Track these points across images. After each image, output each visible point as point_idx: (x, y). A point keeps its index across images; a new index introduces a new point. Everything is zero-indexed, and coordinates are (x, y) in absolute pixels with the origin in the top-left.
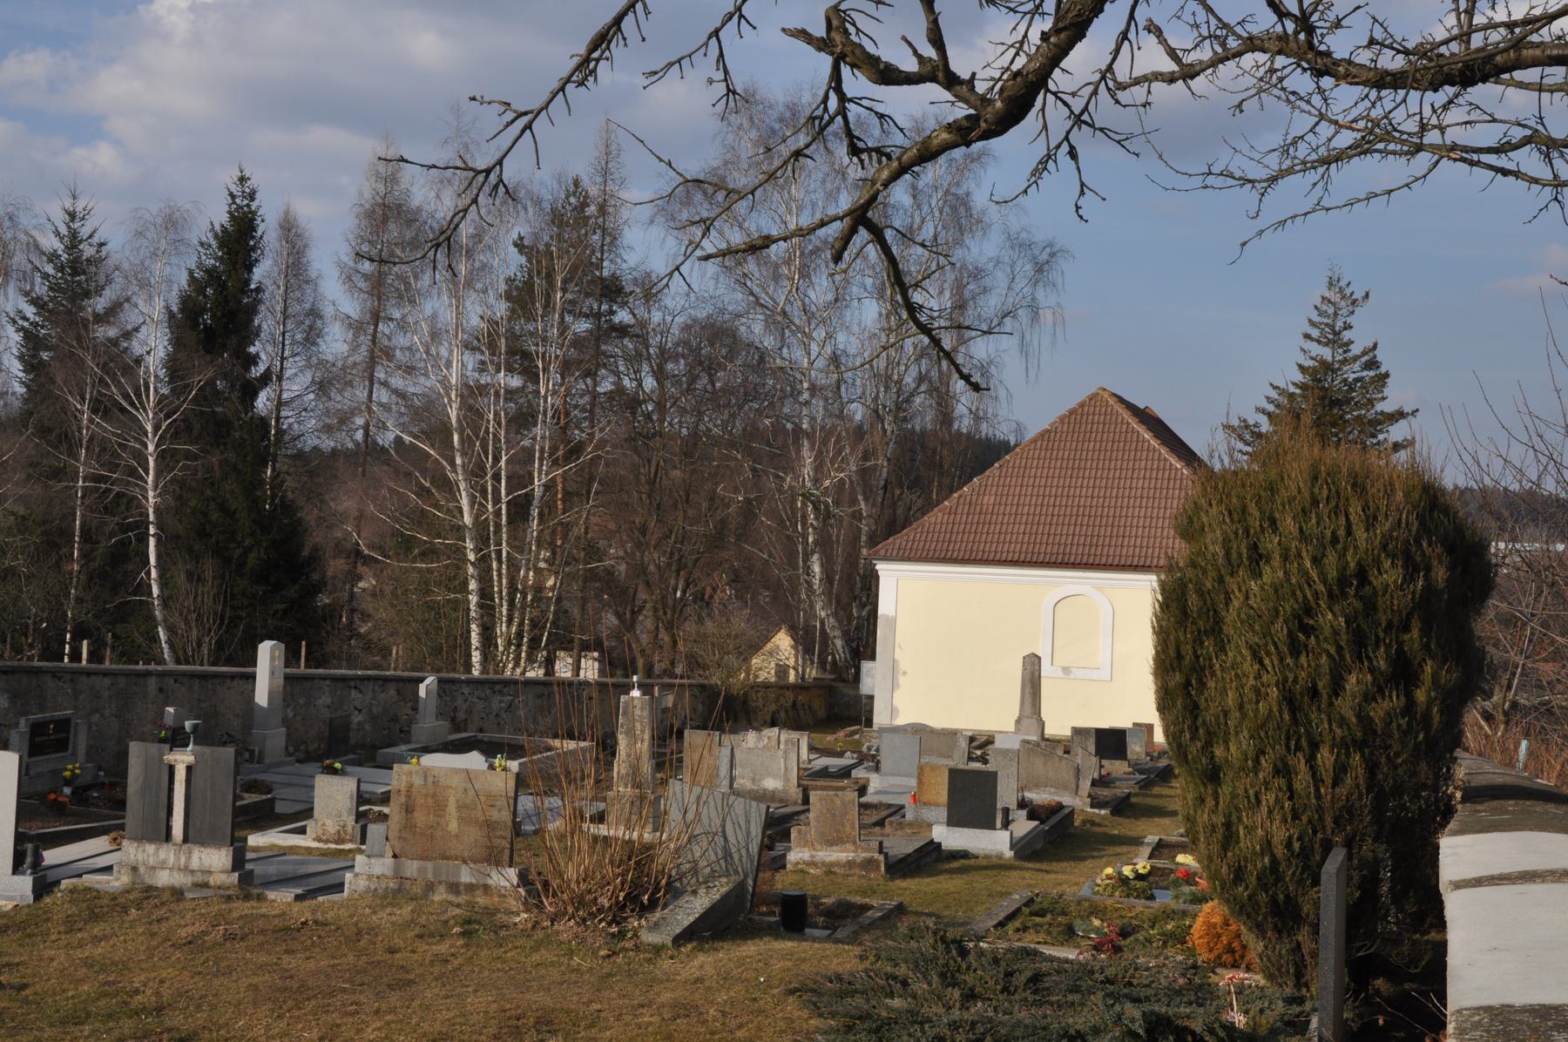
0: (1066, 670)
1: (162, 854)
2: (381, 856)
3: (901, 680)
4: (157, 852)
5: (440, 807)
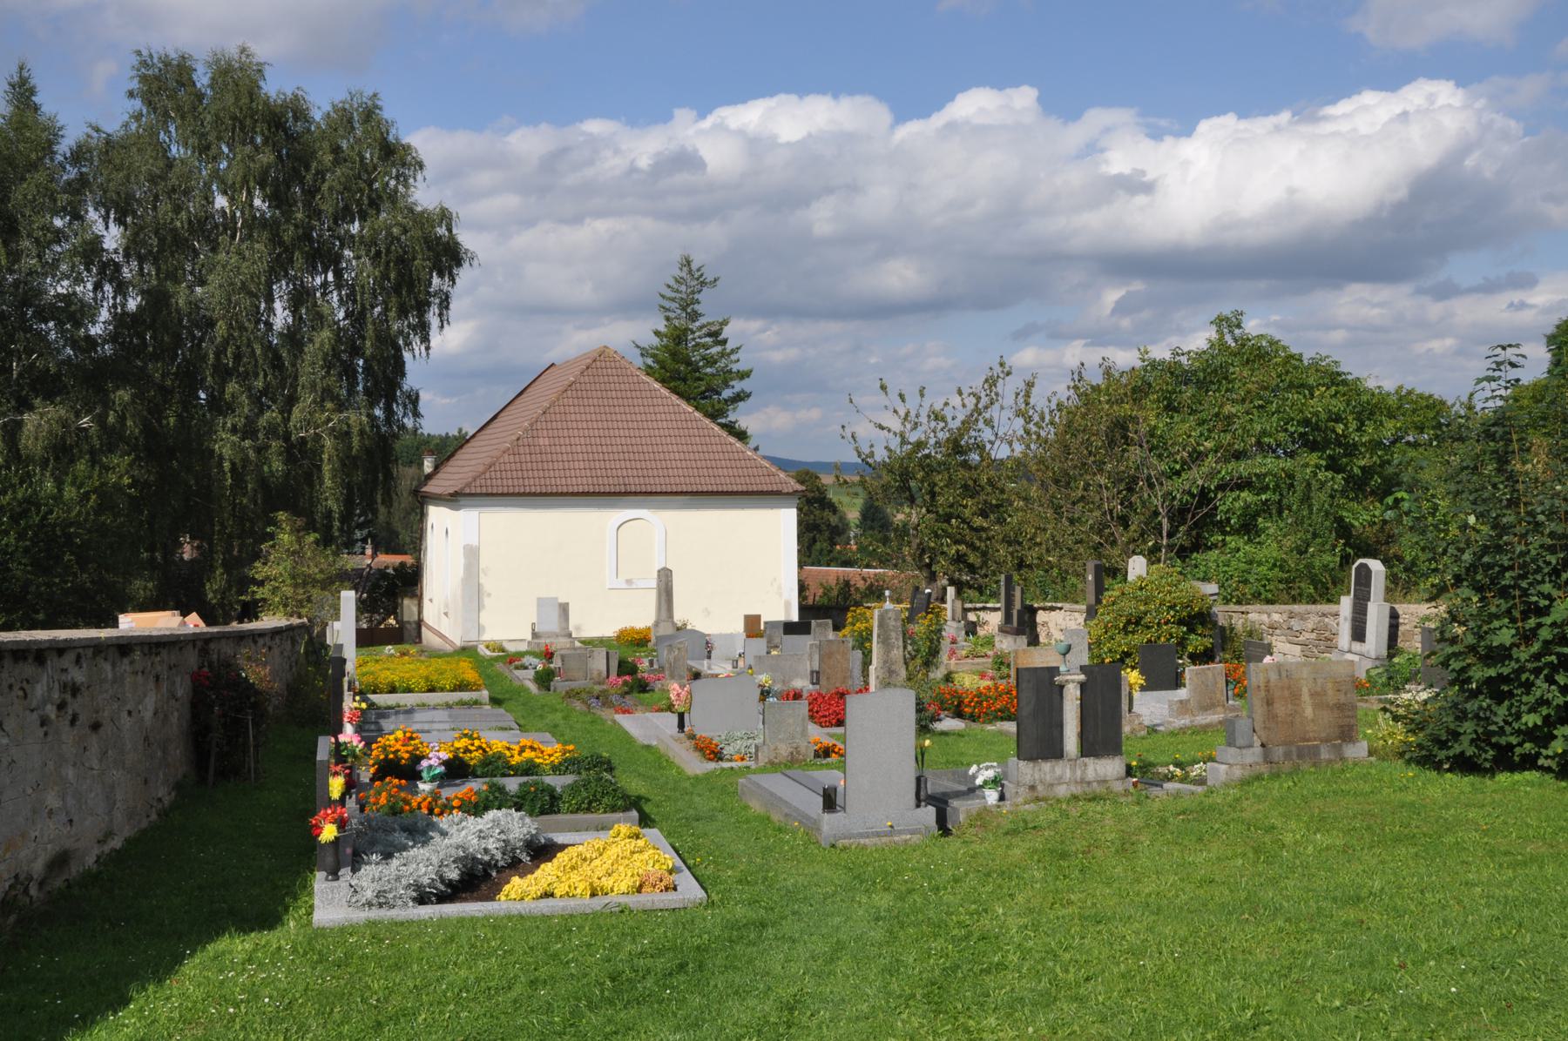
0: (629, 582)
1: (1058, 771)
2: (1251, 746)
3: (486, 601)
4: (1053, 770)
5: (1295, 697)
